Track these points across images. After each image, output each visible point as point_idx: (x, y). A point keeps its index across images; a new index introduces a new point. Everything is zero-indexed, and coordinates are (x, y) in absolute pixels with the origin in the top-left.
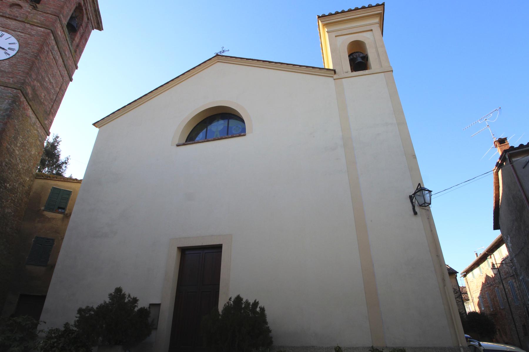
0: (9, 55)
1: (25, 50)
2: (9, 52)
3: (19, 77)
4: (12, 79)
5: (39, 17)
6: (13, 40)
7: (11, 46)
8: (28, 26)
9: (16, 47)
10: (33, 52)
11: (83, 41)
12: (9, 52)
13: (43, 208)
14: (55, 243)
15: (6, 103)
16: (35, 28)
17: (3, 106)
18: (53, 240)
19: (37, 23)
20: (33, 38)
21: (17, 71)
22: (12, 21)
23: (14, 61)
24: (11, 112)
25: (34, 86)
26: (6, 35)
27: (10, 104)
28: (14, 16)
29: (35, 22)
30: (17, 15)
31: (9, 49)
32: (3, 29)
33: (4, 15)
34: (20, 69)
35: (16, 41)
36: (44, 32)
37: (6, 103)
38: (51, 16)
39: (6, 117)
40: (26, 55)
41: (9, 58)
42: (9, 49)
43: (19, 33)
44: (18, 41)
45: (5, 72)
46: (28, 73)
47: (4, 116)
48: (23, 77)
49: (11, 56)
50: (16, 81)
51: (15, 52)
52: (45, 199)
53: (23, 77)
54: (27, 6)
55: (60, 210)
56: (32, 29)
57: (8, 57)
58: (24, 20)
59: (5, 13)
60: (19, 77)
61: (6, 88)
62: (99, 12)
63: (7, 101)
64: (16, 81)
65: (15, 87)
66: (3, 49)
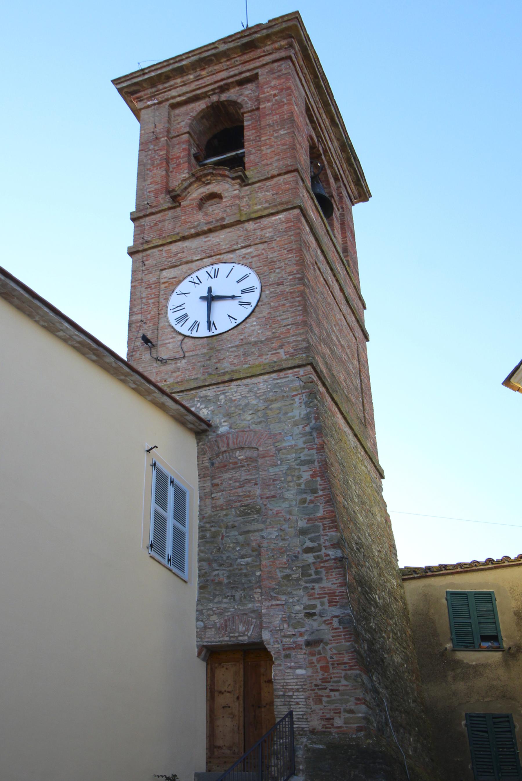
0: (249, 304)
1: (273, 278)
2: (246, 298)
3: (294, 338)
4: (281, 351)
5: (261, 197)
6: (241, 270)
7: (245, 285)
8: (250, 226)
9: (254, 281)
10: (290, 273)
11: (348, 234)
12: (246, 298)
13: (449, 645)
14: (516, 724)
15: (297, 404)
16: (265, 221)
17: (296, 412)
18: (508, 718)
19: (266, 208)
20: (273, 245)
21: (283, 330)
22: (216, 234)
23: (265, 311)
24: (317, 419)
25: (324, 354)
26: (224, 268)
27: (307, 405)
28: (217, 221)
29: (257, 211)
30: (221, 215)
31: (243, 292)
32: (210, 260)
33: (199, 229)
34: (286, 322)
35: (246, 270)
36: (288, 221)
37: (297, 404)
38: (281, 178)
39: (315, 434)
40: (281, 288)
41: (253, 311)
42: (243, 292)
43: (244, 251)
44: (251, 268)
45: (261, 342)
46: (305, 323)
47: (310, 434)
48: (300, 334)
49: (254, 304)
50: (291, 351)
51: (257, 292)
52: (443, 620)
53: (300, 334)
54: (227, 186)
55: (485, 644)
56: (262, 229)
57: (250, 309)
58: (237, 218)
59: (198, 225)
60: (294, 338)
61: (282, 374)
62: (351, 146)
63: (297, 399)
64: (291, 351)
65: (297, 362)
66: (233, 297)
